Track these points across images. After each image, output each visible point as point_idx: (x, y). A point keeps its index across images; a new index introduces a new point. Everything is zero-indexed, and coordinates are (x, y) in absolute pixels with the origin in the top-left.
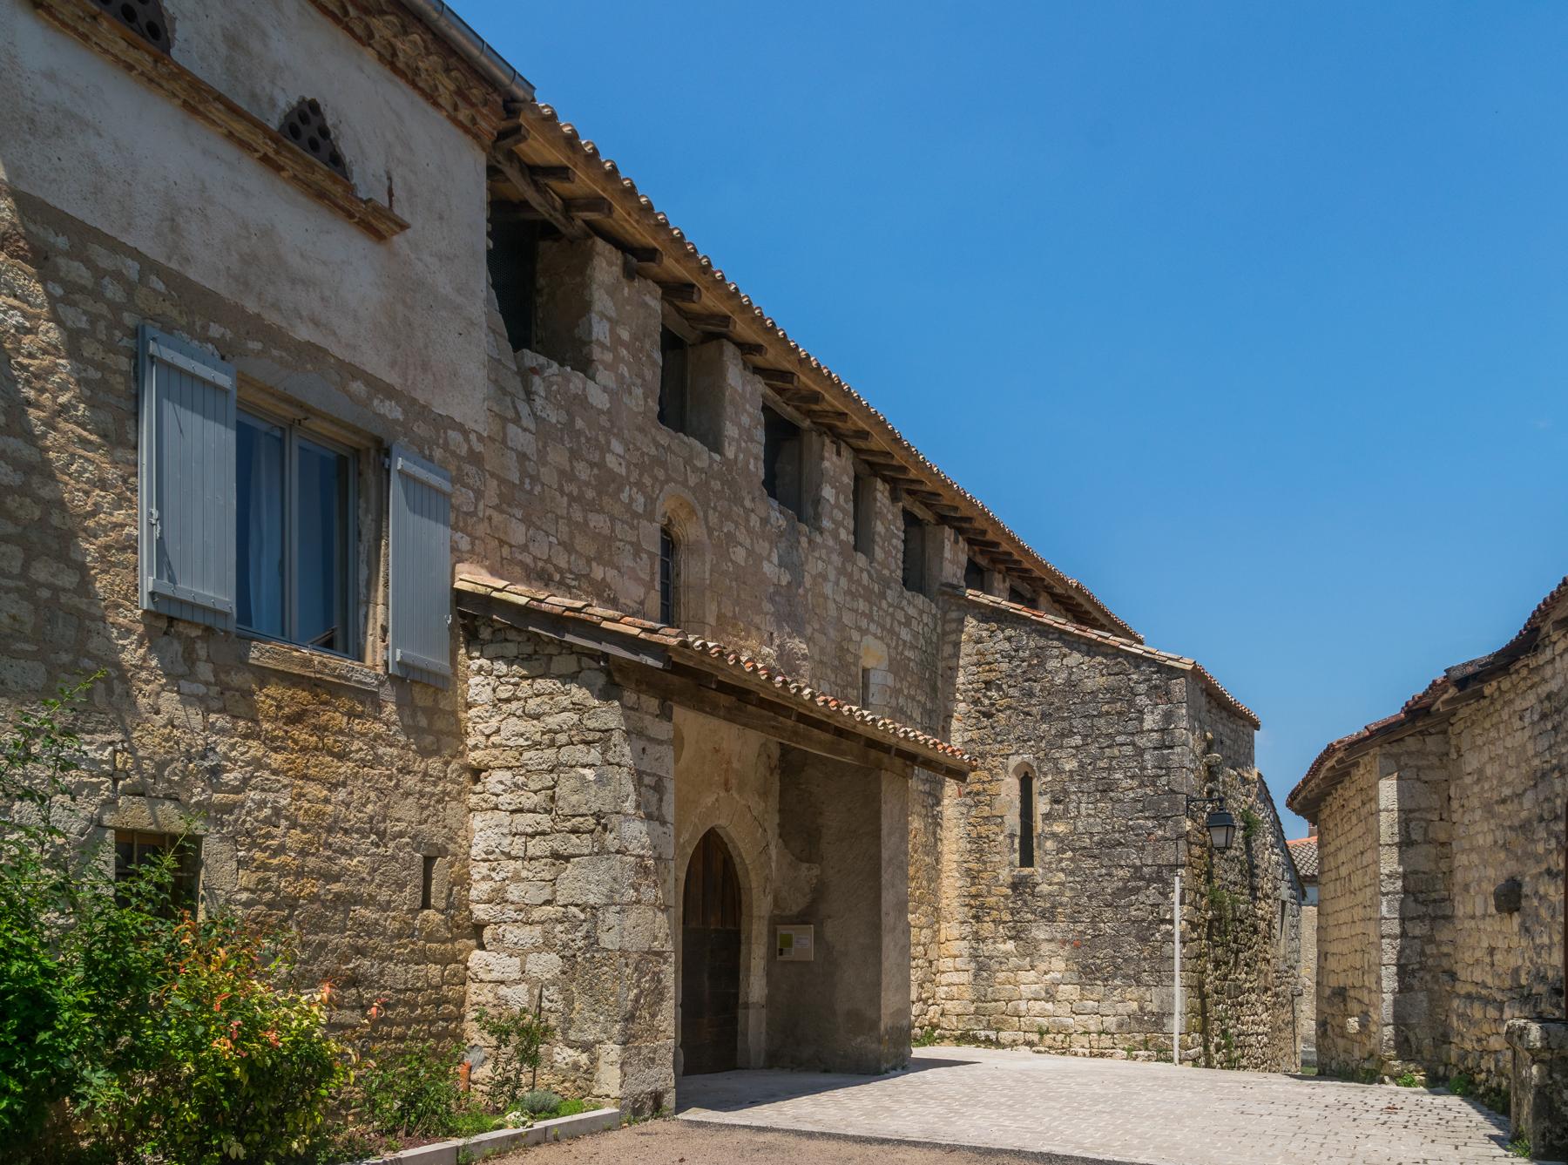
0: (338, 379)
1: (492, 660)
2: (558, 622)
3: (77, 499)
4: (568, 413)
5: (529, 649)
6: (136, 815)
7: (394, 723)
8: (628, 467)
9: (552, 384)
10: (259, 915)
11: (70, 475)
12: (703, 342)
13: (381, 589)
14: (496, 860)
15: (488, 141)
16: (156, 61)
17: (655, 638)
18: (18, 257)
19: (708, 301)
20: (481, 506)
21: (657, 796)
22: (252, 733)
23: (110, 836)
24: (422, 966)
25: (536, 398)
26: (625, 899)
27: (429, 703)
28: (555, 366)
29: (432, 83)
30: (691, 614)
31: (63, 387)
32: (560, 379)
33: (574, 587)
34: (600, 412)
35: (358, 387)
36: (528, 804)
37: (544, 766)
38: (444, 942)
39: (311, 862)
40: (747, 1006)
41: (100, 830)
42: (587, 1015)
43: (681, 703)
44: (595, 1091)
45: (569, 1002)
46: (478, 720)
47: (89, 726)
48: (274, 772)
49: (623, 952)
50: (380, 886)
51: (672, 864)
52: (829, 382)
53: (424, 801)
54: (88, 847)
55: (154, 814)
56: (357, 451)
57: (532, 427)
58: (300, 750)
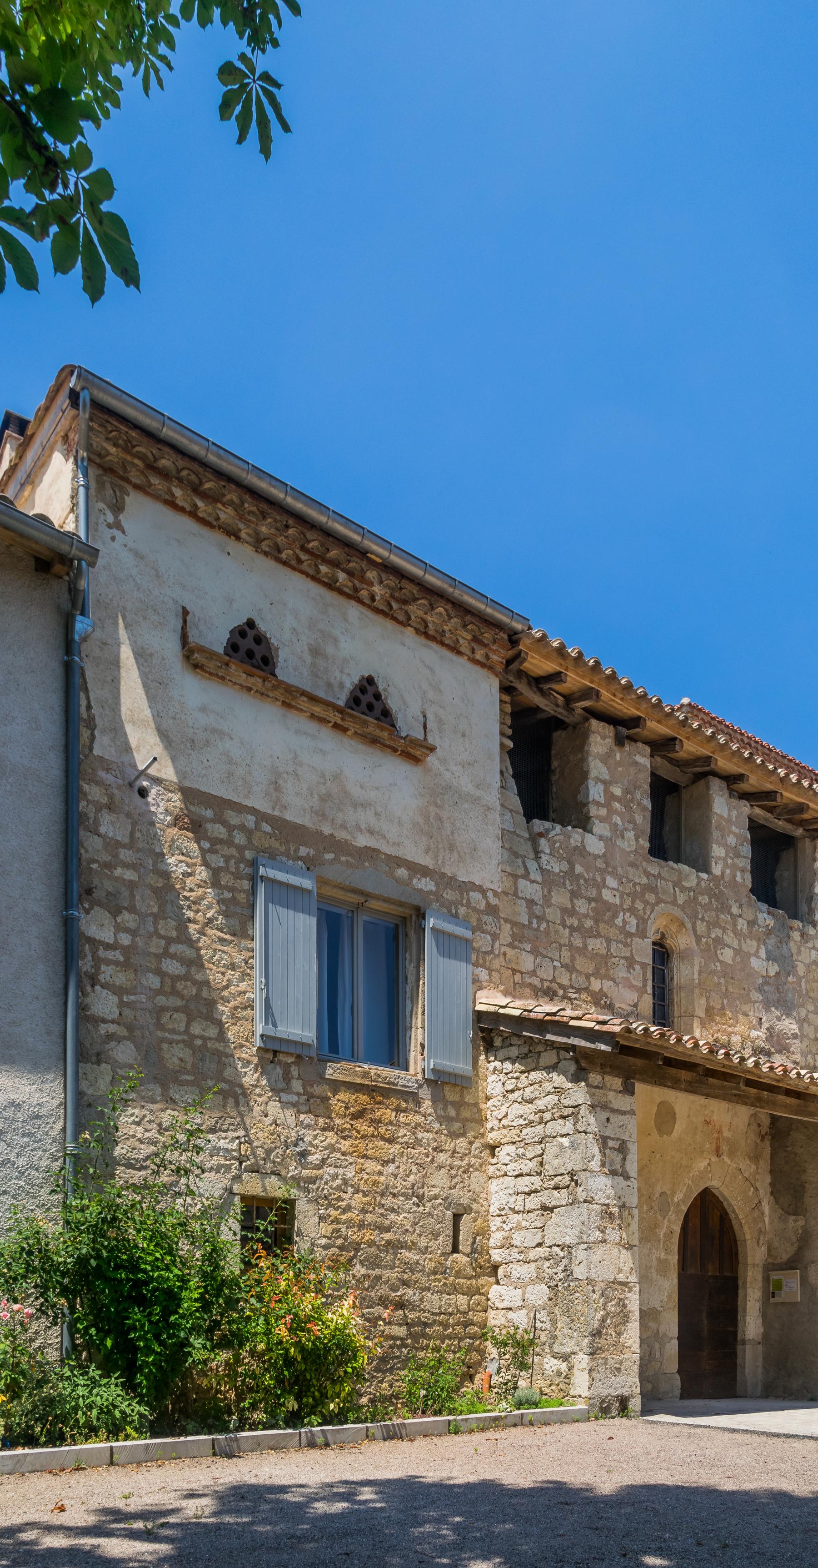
0: (387, 869)
1: (502, 1061)
2: (542, 1025)
3: (216, 977)
4: (569, 863)
5: (525, 1050)
6: (253, 1186)
7: (430, 1115)
8: (621, 897)
9: (555, 842)
10: (333, 1255)
11: (213, 963)
12: (693, 783)
13: (420, 1016)
14: (506, 1215)
15: (499, 668)
16: (264, 681)
17: (605, 1028)
18: (184, 829)
19: (690, 748)
20: (497, 945)
21: (620, 1156)
22: (329, 1126)
23: (237, 1199)
24: (453, 1296)
25: (542, 855)
26: (592, 1239)
27: (457, 1098)
28: (558, 827)
29: (454, 638)
30: (683, 1009)
31: (209, 908)
32: (561, 837)
33: (575, 999)
34: (597, 857)
35: (402, 872)
36: (526, 1170)
37: (536, 1139)
38: (469, 1279)
39: (370, 1218)
40: (744, 1342)
41: (231, 1196)
42: (566, 1332)
43: (643, 1081)
44: (572, 1393)
45: (554, 1322)
46: (494, 1108)
47: (224, 1127)
48: (344, 1154)
49: (590, 1281)
50: (420, 1235)
51: (636, 1212)
52: (811, 793)
53: (453, 1172)
54: (224, 1207)
55: (264, 1186)
56: (405, 918)
57: (539, 879)
58: (361, 1138)
